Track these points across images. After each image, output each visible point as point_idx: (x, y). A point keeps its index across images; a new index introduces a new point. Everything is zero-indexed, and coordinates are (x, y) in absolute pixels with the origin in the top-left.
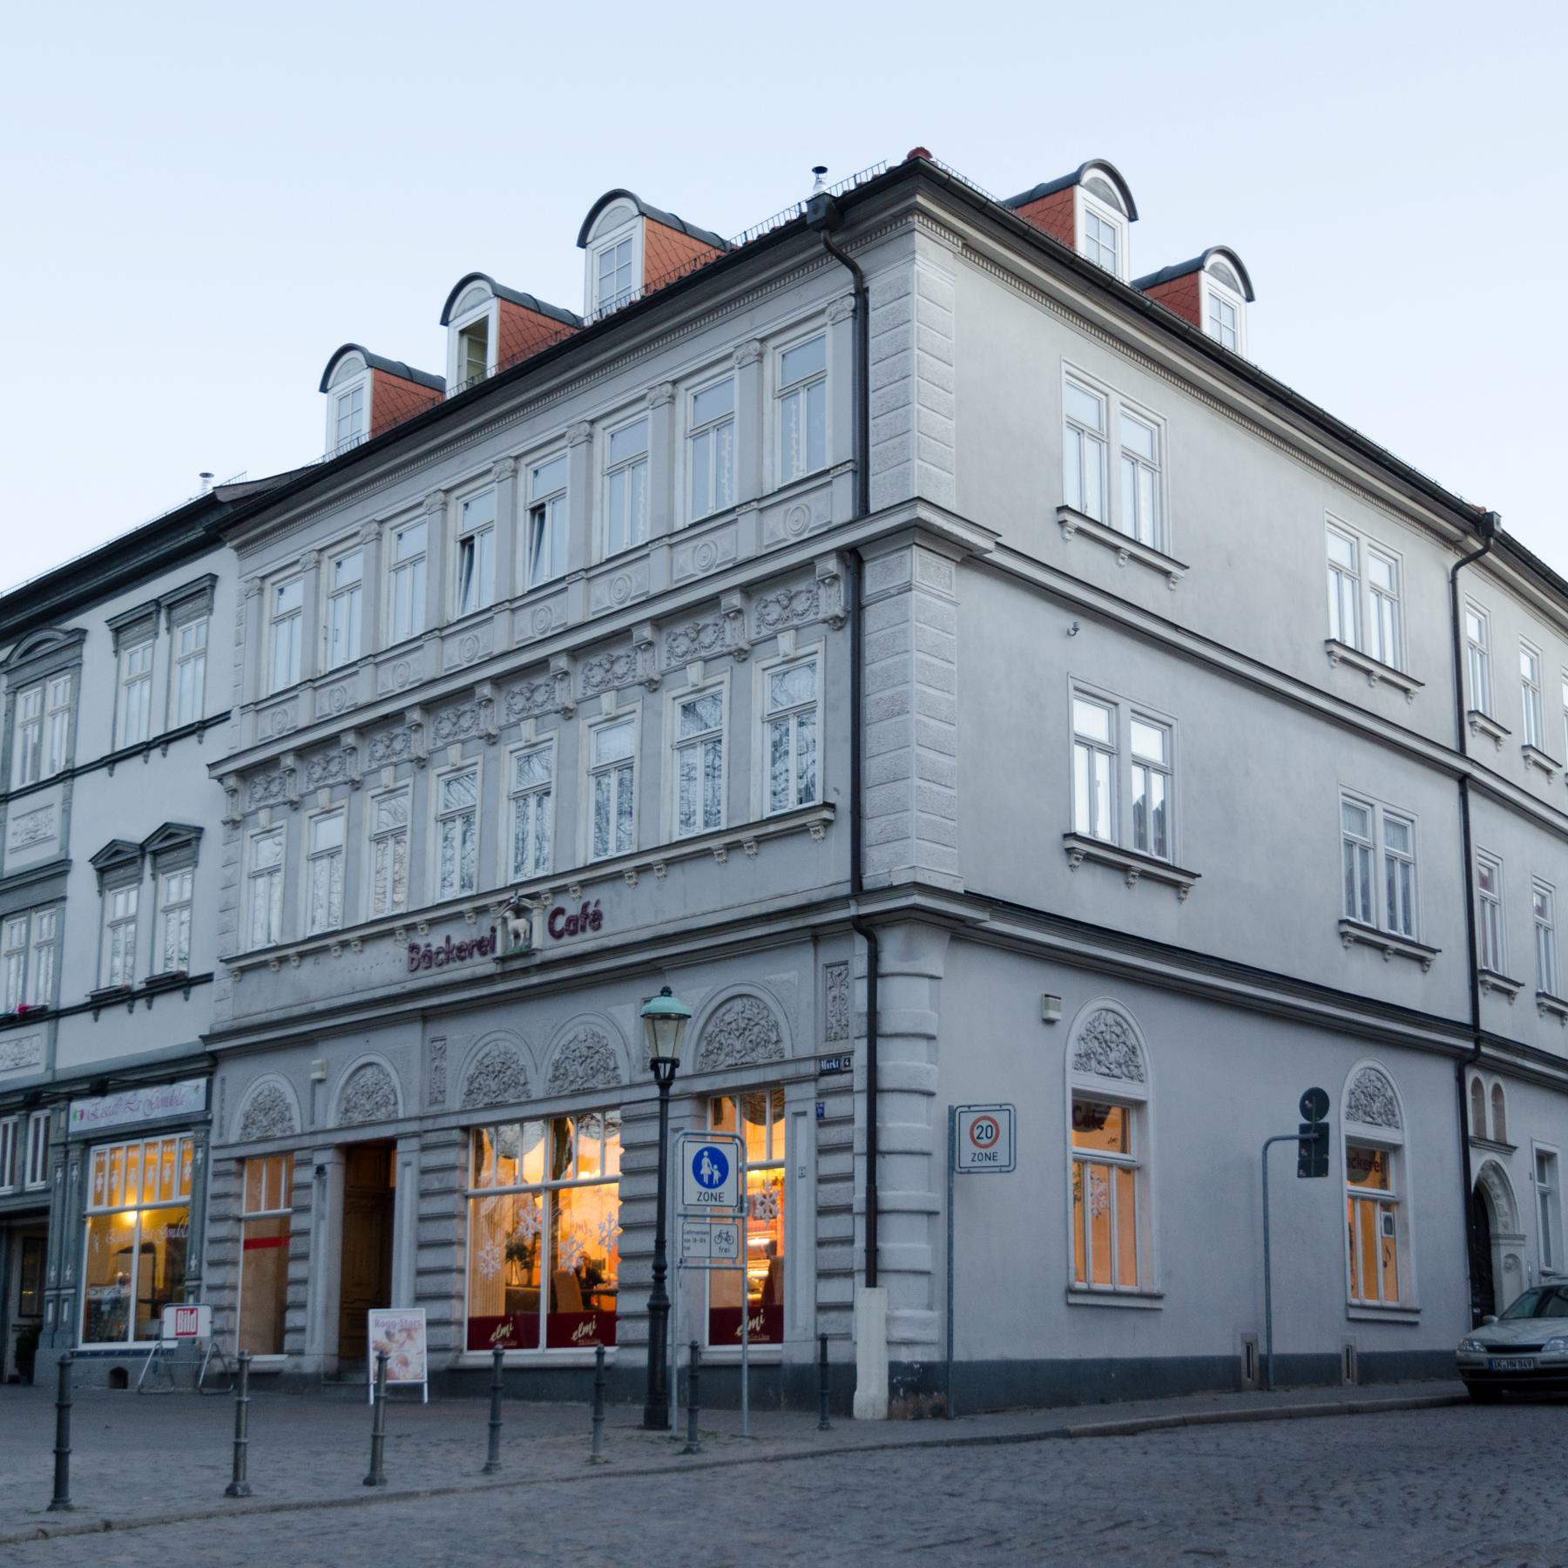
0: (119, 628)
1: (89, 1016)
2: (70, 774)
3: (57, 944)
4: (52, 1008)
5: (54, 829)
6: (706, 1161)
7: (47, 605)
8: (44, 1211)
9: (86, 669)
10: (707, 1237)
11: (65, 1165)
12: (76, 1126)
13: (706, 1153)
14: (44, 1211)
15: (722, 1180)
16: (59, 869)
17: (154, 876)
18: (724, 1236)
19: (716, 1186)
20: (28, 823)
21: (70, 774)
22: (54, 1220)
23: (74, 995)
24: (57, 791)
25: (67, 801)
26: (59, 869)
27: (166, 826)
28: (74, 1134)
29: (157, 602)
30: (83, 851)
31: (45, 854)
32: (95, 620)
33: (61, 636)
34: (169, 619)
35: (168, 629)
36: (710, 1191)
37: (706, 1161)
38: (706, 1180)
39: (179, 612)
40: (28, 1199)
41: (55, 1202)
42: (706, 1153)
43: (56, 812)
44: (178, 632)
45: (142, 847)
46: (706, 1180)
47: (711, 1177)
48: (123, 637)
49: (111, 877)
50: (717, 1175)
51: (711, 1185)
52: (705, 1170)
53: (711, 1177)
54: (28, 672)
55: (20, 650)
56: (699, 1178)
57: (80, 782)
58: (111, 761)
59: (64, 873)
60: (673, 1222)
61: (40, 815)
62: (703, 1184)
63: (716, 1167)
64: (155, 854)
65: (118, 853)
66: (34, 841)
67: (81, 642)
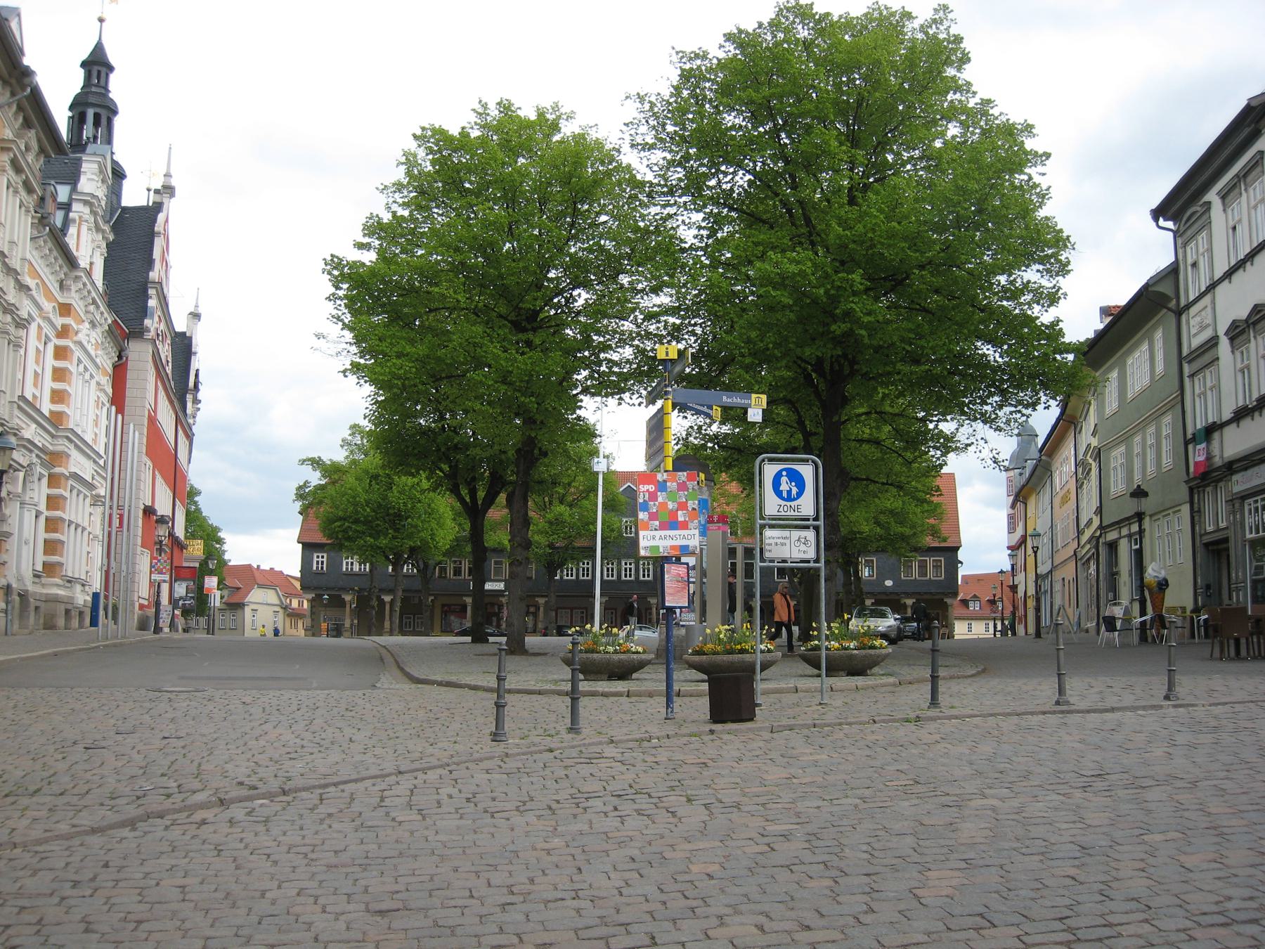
0: (1224, 197)
1: (1234, 425)
2: (1212, 287)
3: (1217, 388)
4: (1219, 422)
5: (1209, 320)
6: (784, 479)
7: (1189, 193)
8: (1226, 540)
9: (1213, 224)
10: (787, 542)
11: (1234, 513)
12: (1236, 489)
13: (784, 473)
14: (1226, 540)
15: (800, 494)
16: (1213, 342)
17: (1255, 337)
18: (803, 540)
19: (794, 499)
20: (1198, 319)
21: (1212, 287)
22: (1232, 544)
23: (1227, 415)
24: (1206, 300)
25: (1213, 302)
26: (1213, 342)
27: (1256, 306)
28: (1236, 493)
29: (1237, 176)
30: (1222, 330)
31: (1207, 334)
32: (1212, 196)
33: (1199, 209)
34: (1245, 184)
35: (1246, 190)
36: (788, 504)
37: (784, 479)
38: (785, 495)
39: (1249, 179)
40: (1220, 533)
41: (1231, 534)
42: (784, 473)
43: (1209, 309)
44: (1251, 190)
45: (1246, 321)
46: (785, 495)
47: (789, 492)
48: (1227, 201)
49: (1237, 341)
50: (795, 490)
51: (789, 499)
52: (784, 487)
53: (789, 492)
54: (1189, 233)
55: (1183, 222)
56: (779, 493)
57: (1219, 290)
58: (1229, 275)
59: (1216, 344)
60: (761, 534)
61: (1203, 313)
62: (783, 499)
63: (793, 484)
64: (1254, 324)
65: (1237, 327)
66: (1203, 328)
67: (1209, 209)
